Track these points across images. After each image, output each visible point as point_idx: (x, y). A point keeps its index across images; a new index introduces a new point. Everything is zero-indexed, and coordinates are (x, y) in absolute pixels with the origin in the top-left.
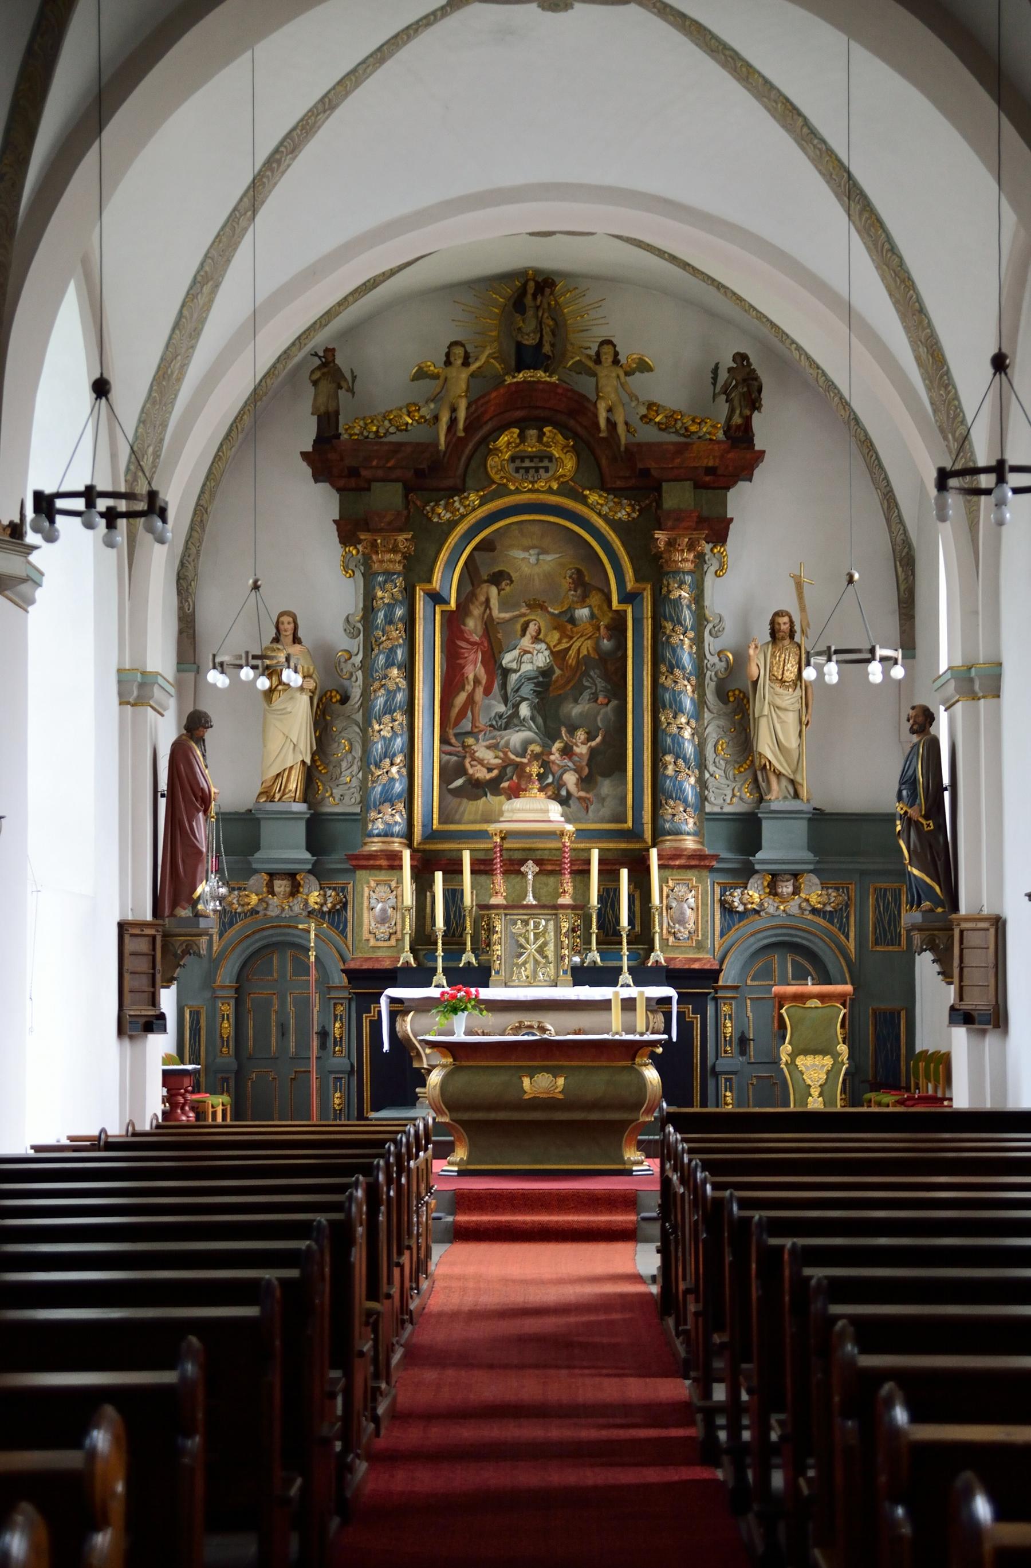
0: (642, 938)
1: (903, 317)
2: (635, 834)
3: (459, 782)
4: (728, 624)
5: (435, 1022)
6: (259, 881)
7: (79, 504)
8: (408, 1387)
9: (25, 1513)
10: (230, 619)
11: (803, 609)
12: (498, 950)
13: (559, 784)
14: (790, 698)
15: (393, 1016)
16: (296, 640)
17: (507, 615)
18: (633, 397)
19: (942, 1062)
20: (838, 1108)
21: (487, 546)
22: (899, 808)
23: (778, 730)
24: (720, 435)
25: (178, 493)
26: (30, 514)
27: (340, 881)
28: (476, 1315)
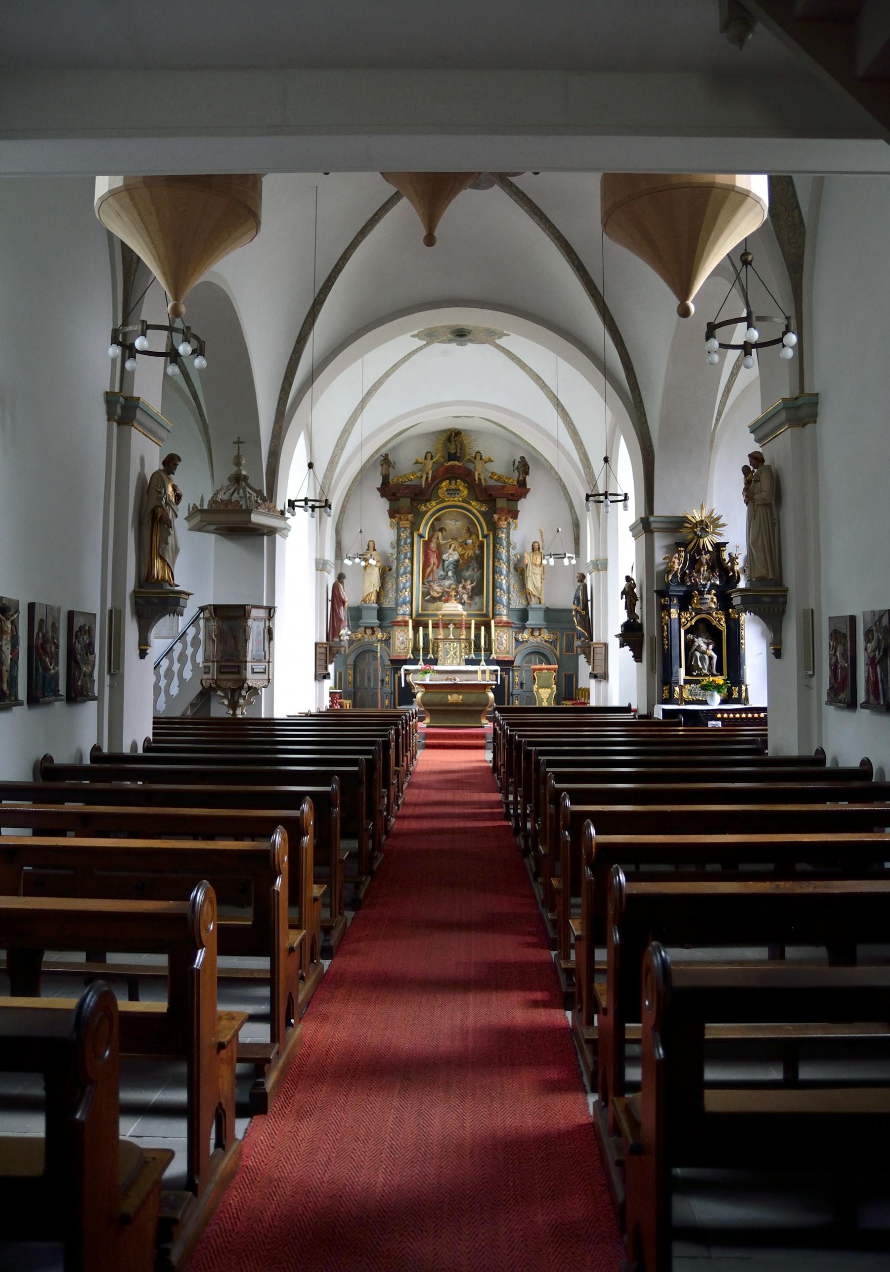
0: (489, 650)
1: (575, 445)
2: (486, 615)
5: (419, 677)
6: (361, 630)
7: (303, 504)
8: (409, 795)
9: (280, 829)
12: (441, 653)
13: (461, 598)
14: (538, 570)
15: (405, 675)
16: (374, 550)
18: (487, 470)
19: (587, 691)
20: (553, 705)
21: (438, 519)
22: (574, 607)
23: (534, 581)
24: (516, 483)
25: (336, 502)
26: (287, 507)
27: (388, 630)
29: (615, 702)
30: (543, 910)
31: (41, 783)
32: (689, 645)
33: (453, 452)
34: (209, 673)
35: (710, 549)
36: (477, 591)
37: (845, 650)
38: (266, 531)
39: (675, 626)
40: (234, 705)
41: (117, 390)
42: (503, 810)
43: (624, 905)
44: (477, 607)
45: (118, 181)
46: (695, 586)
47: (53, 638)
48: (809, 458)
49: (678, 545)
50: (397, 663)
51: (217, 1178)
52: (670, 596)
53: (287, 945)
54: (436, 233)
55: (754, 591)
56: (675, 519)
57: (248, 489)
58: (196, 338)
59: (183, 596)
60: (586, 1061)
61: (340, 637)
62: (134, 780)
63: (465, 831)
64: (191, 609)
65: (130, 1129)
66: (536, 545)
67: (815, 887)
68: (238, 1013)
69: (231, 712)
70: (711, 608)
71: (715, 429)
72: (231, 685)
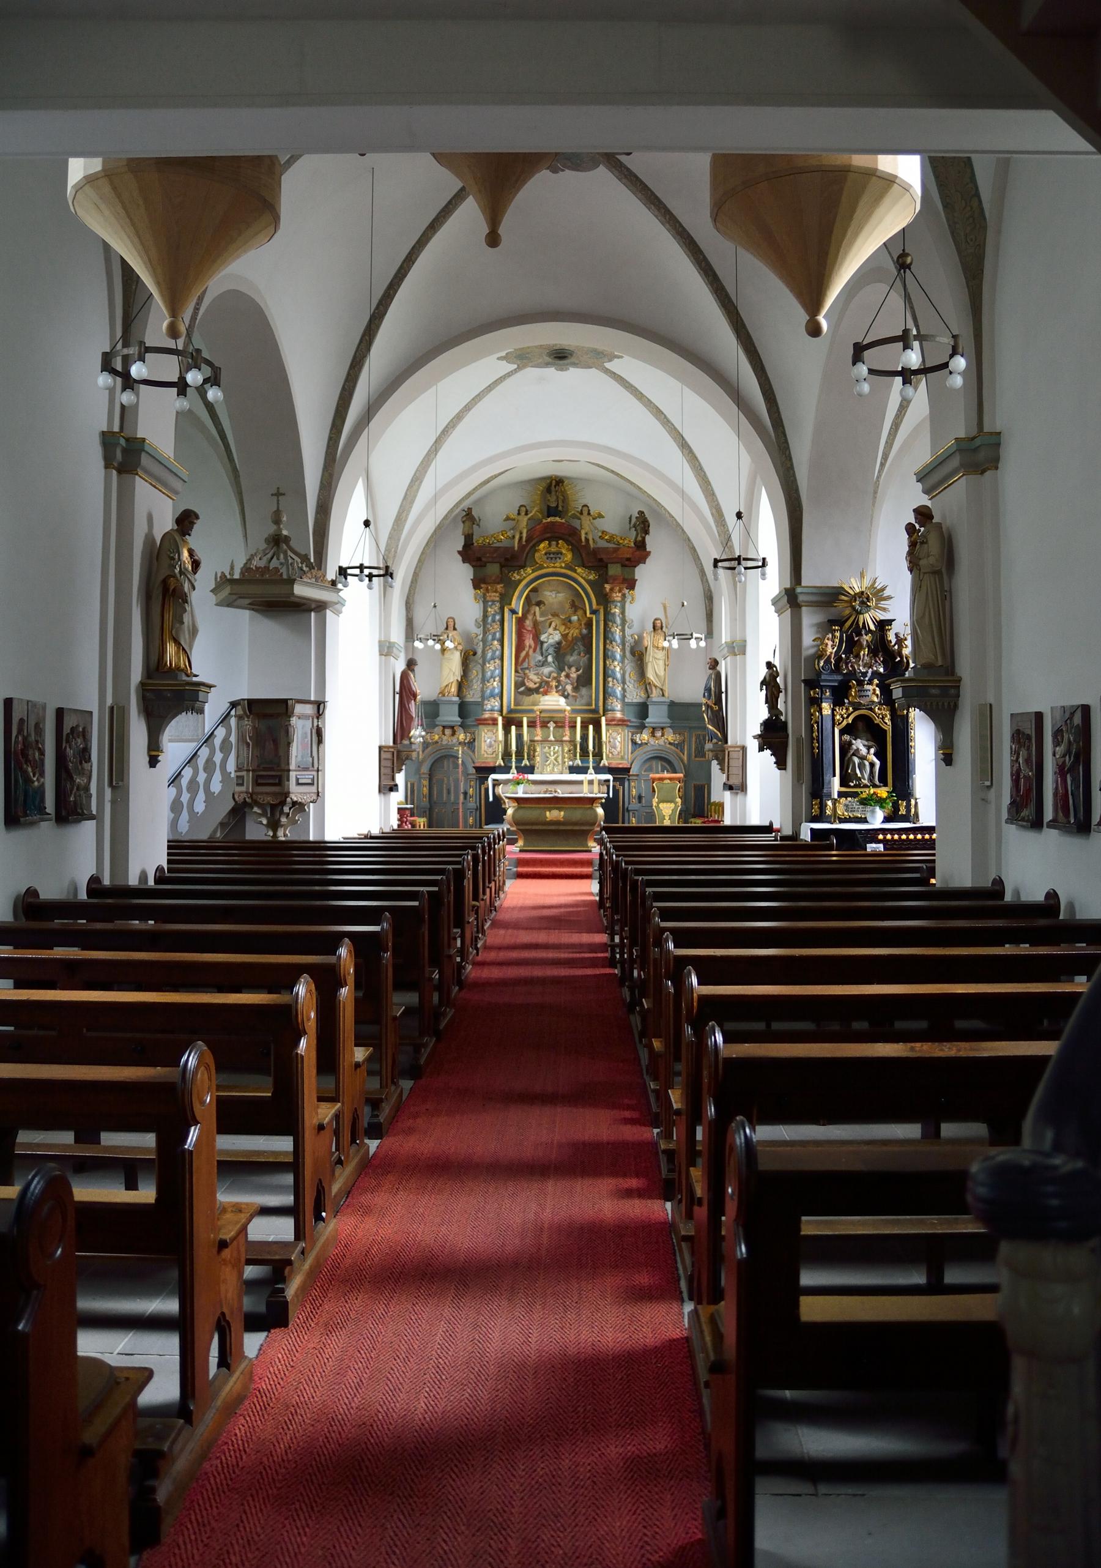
0: (598, 754)
1: (706, 497)
2: (596, 711)
3: (522, 689)
4: (636, 625)
5: (510, 788)
6: (439, 729)
7: (357, 571)
8: (493, 936)
10: (426, 622)
11: (666, 617)
12: (538, 759)
13: (564, 690)
15: (494, 786)
16: (455, 629)
17: (542, 619)
18: (596, 528)
19: (721, 806)
20: (676, 824)
21: (535, 590)
22: (704, 701)
23: (655, 669)
27: (473, 730)
28: (523, 908)
29: (755, 820)
30: (647, 1078)
31: (23, 923)
32: (845, 748)
33: (553, 503)
34: (242, 785)
35: (872, 627)
36: (584, 681)
37: (1030, 755)
38: (313, 606)
39: (828, 724)
40: (274, 825)
41: (116, 429)
42: (608, 955)
43: (720, 1071)
44: (584, 701)
45: (96, 165)
46: (852, 674)
47: (37, 742)
48: (989, 514)
49: (831, 622)
50: (484, 772)
51: (219, 1402)
52: (821, 687)
53: (315, 1122)
54: (502, 230)
55: (920, 681)
56: (827, 591)
57: (290, 553)
58: (209, 363)
59: (203, 688)
60: (684, 1263)
61: (410, 738)
62: (144, 918)
63: (557, 981)
64: (214, 706)
65: (90, 1344)
66: (658, 623)
67: (959, 1050)
68: (247, 1204)
69: (271, 833)
70: (873, 702)
71: (879, 477)
72: (269, 799)
